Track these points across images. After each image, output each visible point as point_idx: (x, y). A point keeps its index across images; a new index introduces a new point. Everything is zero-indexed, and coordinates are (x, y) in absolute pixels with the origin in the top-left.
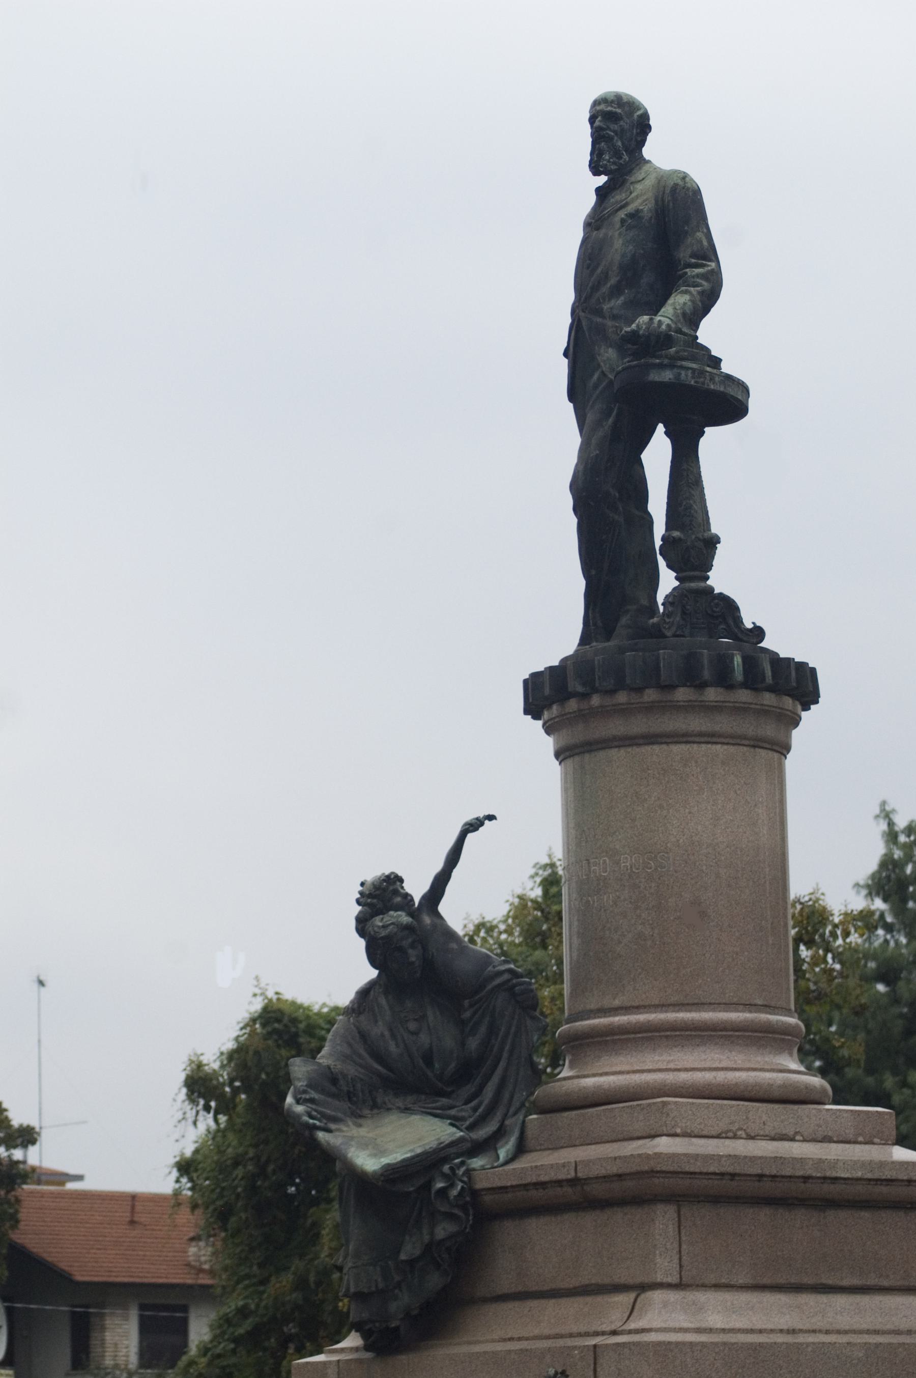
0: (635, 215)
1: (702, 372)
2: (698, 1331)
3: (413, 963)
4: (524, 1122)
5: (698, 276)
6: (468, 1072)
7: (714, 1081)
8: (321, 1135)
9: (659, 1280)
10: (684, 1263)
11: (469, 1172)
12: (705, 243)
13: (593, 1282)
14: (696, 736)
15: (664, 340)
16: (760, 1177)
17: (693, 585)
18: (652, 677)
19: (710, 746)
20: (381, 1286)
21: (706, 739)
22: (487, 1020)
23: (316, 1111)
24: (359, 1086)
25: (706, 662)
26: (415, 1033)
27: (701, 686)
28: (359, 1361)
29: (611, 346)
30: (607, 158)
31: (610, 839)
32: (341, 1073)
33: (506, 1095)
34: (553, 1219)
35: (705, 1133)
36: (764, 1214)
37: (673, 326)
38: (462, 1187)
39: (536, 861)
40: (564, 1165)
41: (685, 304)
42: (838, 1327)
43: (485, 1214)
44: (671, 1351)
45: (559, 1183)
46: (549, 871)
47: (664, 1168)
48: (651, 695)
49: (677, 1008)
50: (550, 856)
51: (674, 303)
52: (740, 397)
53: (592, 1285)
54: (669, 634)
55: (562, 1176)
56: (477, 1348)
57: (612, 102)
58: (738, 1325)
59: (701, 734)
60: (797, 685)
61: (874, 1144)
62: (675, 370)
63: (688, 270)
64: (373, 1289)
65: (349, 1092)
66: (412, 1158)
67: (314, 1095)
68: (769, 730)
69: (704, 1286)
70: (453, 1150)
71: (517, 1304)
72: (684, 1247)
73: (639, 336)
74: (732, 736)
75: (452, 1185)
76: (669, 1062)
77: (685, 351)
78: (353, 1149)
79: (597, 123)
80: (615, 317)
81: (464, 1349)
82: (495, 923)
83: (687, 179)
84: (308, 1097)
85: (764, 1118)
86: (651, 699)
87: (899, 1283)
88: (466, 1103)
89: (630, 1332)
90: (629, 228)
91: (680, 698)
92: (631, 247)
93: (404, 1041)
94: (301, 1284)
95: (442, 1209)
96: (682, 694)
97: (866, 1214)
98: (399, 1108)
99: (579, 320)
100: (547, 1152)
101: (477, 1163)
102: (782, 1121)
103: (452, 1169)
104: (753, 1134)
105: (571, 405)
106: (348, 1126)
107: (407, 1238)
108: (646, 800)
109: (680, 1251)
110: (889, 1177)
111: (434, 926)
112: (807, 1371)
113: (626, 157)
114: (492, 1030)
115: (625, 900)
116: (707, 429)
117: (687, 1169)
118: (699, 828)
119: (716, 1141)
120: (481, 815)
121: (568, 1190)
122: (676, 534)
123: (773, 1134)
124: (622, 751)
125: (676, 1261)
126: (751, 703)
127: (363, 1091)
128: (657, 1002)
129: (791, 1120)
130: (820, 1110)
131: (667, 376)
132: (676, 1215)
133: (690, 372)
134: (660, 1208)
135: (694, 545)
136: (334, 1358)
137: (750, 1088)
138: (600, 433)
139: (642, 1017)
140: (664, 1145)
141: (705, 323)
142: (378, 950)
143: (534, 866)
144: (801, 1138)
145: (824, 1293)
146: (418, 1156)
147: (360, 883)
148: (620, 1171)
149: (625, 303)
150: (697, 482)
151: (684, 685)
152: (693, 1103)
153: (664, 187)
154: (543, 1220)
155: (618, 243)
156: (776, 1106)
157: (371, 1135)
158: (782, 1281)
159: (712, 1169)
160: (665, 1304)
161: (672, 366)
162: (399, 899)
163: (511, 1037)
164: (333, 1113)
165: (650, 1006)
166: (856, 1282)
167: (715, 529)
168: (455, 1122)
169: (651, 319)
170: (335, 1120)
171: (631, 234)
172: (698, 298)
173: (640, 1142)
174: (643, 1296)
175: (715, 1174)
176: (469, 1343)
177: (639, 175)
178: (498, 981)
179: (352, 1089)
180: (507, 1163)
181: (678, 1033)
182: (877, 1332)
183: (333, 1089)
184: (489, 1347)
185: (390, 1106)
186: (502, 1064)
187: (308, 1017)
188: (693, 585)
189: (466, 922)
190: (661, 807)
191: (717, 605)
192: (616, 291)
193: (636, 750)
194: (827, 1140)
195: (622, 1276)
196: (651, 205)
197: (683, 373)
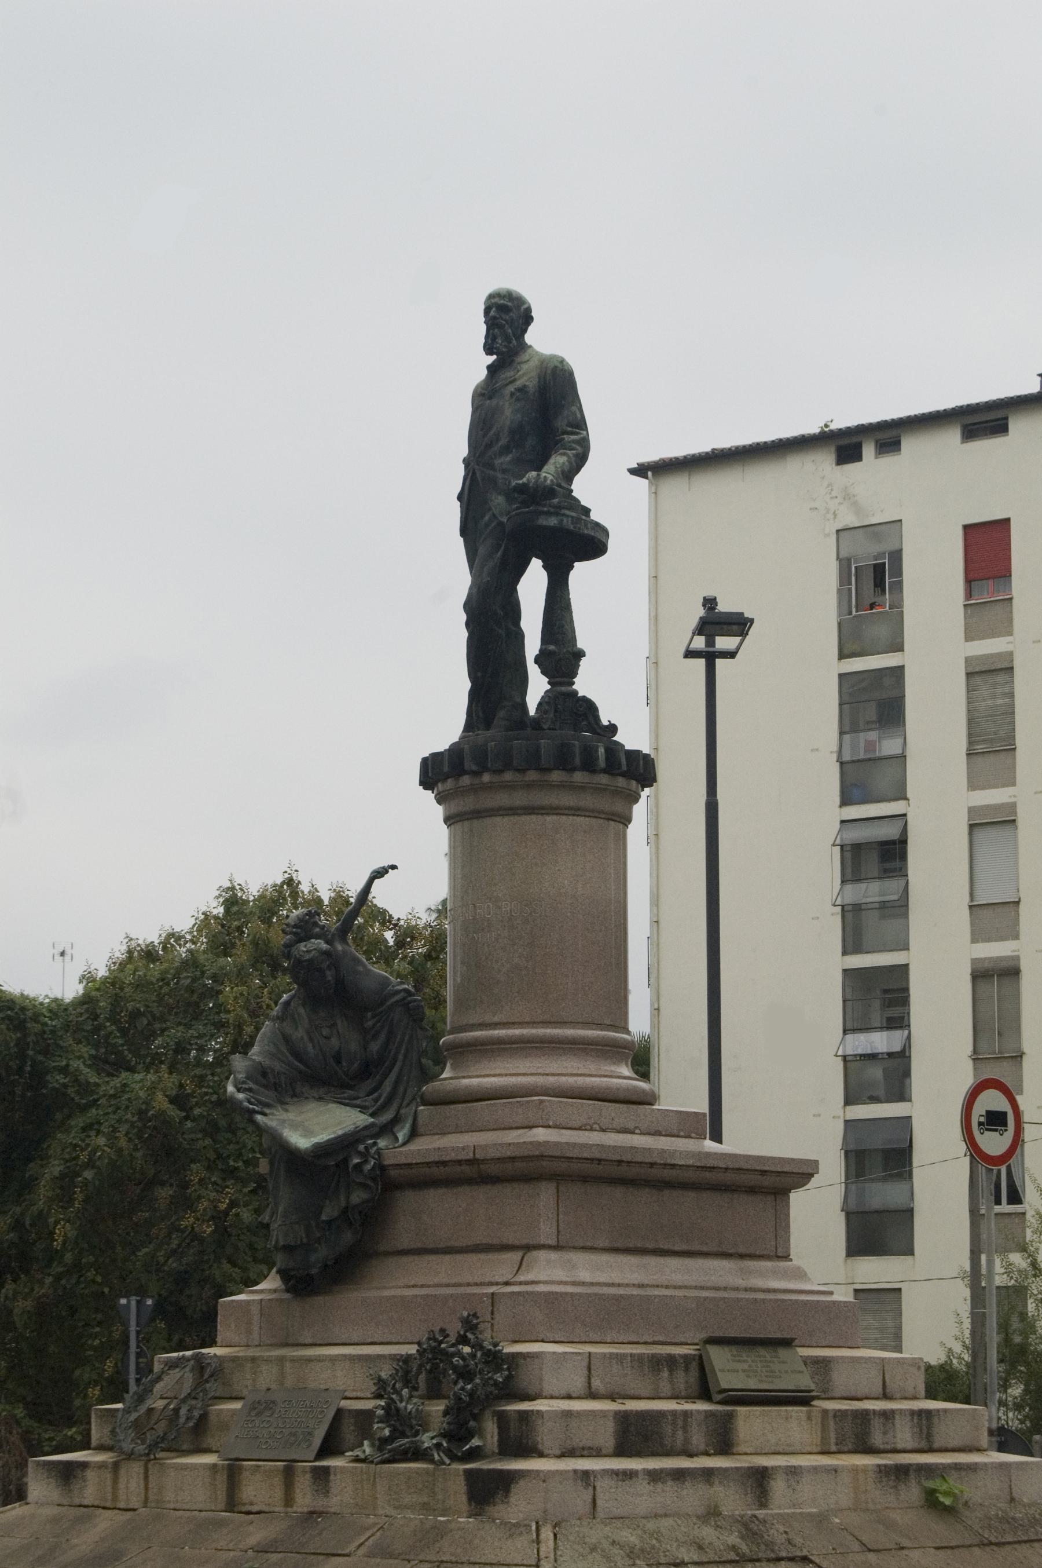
0: (522, 390)
1: (579, 519)
2: (574, 1284)
4: (416, 1111)
5: (574, 441)
11: (379, 1152)
12: (579, 415)
15: (549, 492)
17: (563, 689)
18: (533, 761)
24: (283, 1078)
25: (577, 751)
27: (573, 770)
28: (281, 1301)
29: (500, 494)
33: (401, 1089)
36: (619, 1192)
40: (463, 1148)
43: (390, 1183)
45: (459, 1162)
48: (532, 776)
54: (545, 727)
55: (462, 1156)
56: (386, 1293)
58: (602, 1280)
59: (570, 808)
62: (560, 518)
65: (275, 1083)
66: (335, 1138)
67: (251, 1085)
68: (618, 807)
70: (365, 1133)
72: (561, 1216)
74: (592, 811)
75: (366, 1161)
79: (492, 313)
80: (504, 471)
89: (521, 1283)
90: (518, 400)
94: (18, 1225)
96: (556, 776)
98: (314, 1097)
99: (474, 473)
100: (437, 1137)
101: (382, 1143)
108: (524, 859)
113: (514, 342)
116: (576, 564)
121: (466, 1168)
122: (552, 647)
124: (506, 818)
125: (555, 1227)
131: (553, 521)
134: (543, 1185)
135: (562, 656)
136: (257, 1297)
138: (491, 564)
139: (517, 1032)
140: (540, 1134)
141: (577, 479)
146: (339, 1137)
148: (513, 1155)
150: (567, 607)
151: (558, 769)
154: (441, 1191)
155: (508, 412)
156: (621, 1106)
157: (299, 1119)
159: (585, 1155)
161: (557, 514)
162: (318, 930)
166: (684, 1247)
167: (580, 644)
168: (363, 1109)
169: (539, 475)
170: (268, 1105)
172: (573, 459)
173: (520, 1131)
174: (529, 1254)
177: (525, 357)
178: (396, 998)
180: (404, 1144)
182: (702, 1288)
183: (264, 1082)
184: (399, 1292)
185: (306, 1095)
186: (399, 1064)
187: (34, 1006)
188: (563, 689)
190: (536, 864)
192: (506, 450)
194: (657, 1133)
195: (510, 1238)
196: (535, 382)
197: (565, 521)
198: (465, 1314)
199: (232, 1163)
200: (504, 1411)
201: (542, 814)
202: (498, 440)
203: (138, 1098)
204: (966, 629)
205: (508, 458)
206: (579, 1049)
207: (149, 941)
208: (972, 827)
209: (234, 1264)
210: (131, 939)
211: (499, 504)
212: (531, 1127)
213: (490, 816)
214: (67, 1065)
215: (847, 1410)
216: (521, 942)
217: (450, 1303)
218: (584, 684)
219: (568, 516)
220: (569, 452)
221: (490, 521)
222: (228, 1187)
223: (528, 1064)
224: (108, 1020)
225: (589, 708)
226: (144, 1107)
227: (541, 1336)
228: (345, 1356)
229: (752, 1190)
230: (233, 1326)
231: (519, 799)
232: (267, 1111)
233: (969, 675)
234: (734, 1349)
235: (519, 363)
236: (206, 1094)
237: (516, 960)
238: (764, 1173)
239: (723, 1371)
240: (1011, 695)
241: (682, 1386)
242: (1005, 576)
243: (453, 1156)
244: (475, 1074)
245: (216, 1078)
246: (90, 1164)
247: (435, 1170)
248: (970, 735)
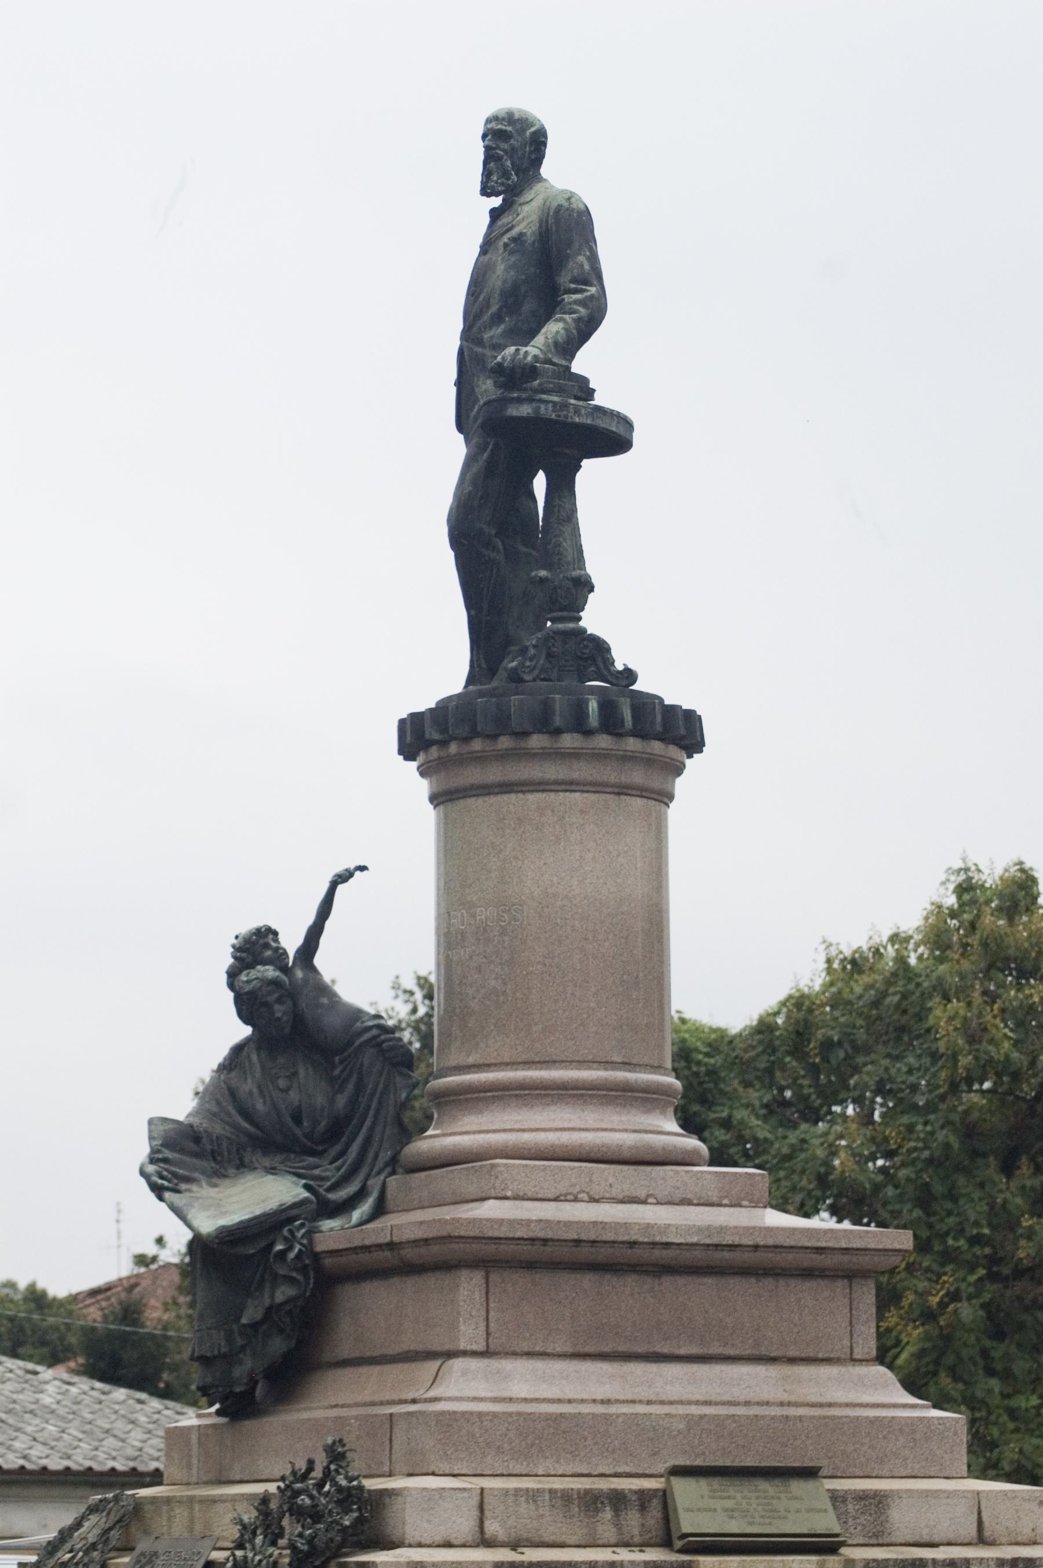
0: (518, 239)
1: (565, 406)
2: (495, 1400)
3: (279, 1019)
5: (576, 302)
6: (337, 1131)
7: (557, 1142)
9: (462, 1348)
10: (491, 1330)
13: (412, 1348)
15: (530, 371)
16: (578, 1242)
19: (568, 794)
20: (223, 1350)
23: (167, 1170)
24: (225, 1144)
26: (286, 1091)
27: (558, 732)
30: (495, 178)
31: (467, 891)
32: (206, 1131)
35: (540, 1196)
36: (587, 1280)
37: (541, 356)
38: (300, 1250)
39: (949, 866)
41: (557, 332)
42: (664, 1398)
43: (327, 1280)
44: (456, 1420)
45: (380, 1246)
46: (963, 877)
47: (462, 1233)
49: (514, 1067)
50: (964, 860)
51: (546, 333)
52: (614, 429)
54: (527, 678)
57: (503, 119)
59: (556, 782)
60: (683, 732)
61: (741, 1206)
62: (534, 405)
63: (565, 296)
64: (216, 1353)
65: (213, 1152)
67: (167, 1154)
69: (515, 1354)
72: (492, 1313)
74: (591, 784)
75: (290, 1248)
76: (516, 1122)
77: (550, 383)
78: (193, 1211)
81: (305, 1415)
82: (910, 933)
83: (573, 200)
84: (160, 1156)
85: (611, 1180)
86: (504, 746)
87: (747, 1352)
88: (332, 1163)
90: (511, 253)
91: (534, 746)
92: (512, 273)
93: (271, 1096)
95: (281, 1272)
96: (537, 741)
97: (709, 1281)
102: (632, 1184)
103: (291, 1231)
104: (597, 1197)
105: (462, 436)
106: (201, 1187)
107: (250, 1301)
108: (501, 851)
109: (487, 1319)
110: (730, 1242)
111: (306, 981)
112: (616, 1442)
113: (514, 177)
114: (359, 1088)
117: (490, 1234)
118: (555, 880)
119: (553, 1204)
120: (352, 866)
121: (387, 1254)
123: (621, 1196)
124: (480, 800)
126: (612, 750)
127: (229, 1153)
129: (642, 1183)
130: (677, 1172)
131: (525, 410)
132: (484, 1281)
133: (550, 405)
134: (464, 1274)
137: (595, 1149)
138: (475, 469)
140: (490, 1210)
141: (580, 355)
142: (247, 1005)
143: (947, 871)
144: (654, 1201)
145: (655, 1362)
148: (425, 1236)
151: (540, 732)
152: (527, 1165)
153: (549, 209)
155: (500, 268)
156: (625, 1168)
158: (606, 1349)
160: (465, 1373)
161: (530, 400)
163: (377, 1095)
164: (186, 1173)
165: (501, 1064)
169: (517, 350)
170: (188, 1180)
171: (513, 259)
172: (573, 325)
178: (367, 1036)
179: (216, 1148)
181: (527, 1092)
186: (368, 1123)
189: (871, 933)
190: (516, 858)
191: (586, 647)
196: (535, 227)
197: (543, 407)
198: (330, 1440)
199: (950, 1242)
200: (345, 1562)
201: (523, 792)
202: (488, 306)
203: (814, 1157)
206: (574, 1096)
207: (855, 947)
209: (956, 1378)
210: (831, 945)
213: (464, 797)
214: (730, 1117)
215: (887, 1560)
219: (547, 402)
220: (567, 317)
222: (945, 1274)
224: (788, 1053)
226: (822, 1170)
227: (432, 1468)
228: (243, 1495)
229: (809, 1273)
231: (494, 774)
234: (716, 1482)
235: (521, 204)
236: (915, 1149)
237: (493, 983)
238: (819, 1250)
239: (688, 1510)
241: (636, 1531)
245: (929, 1128)
247: (365, 1257)
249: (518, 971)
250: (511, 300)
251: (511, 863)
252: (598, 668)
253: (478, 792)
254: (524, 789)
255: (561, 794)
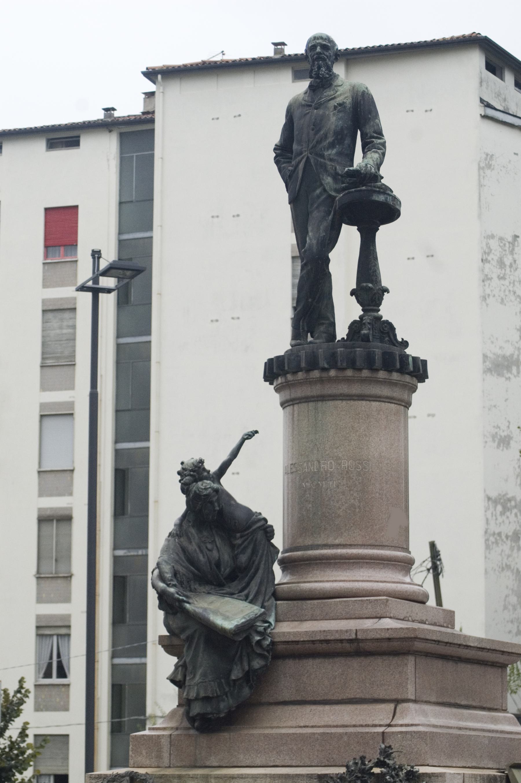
5: (380, 144)
8: (187, 606)
10: (417, 689)
14: (384, 398)
19: (389, 404)
21: (374, 399)
22: (251, 546)
29: (329, 175)
30: (324, 70)
31: (335, 450)
33: (263, 589)
34: (326, 661)
36: (439, 663)
40: (347, 631)
53: (356, 698)
57: (326, 39)
59: (387, 397)
62: (386, 196)
66: (246, 622)
71: (299, 707)
72: (417, 679)
73: (361, 173)
75: (264, 639)
80: (331, 160)
86: (366, 375)
90: (339, 111)
98: (204, 592)
108: (357, 431)
114: (254, 552)
115: (344, 485)
124: (344, 402)
125: (414, 687)
128: (361, 543)
147: (180, 462)
148: (391, 637)
149: (336, 153)
155: (333, 119)
167: (384, 283)
171: (341, 115)
175: (434, 641)
176: (262, 728)
181: (373, 561)
190: (366, 435)
192: (332, 145)
193: (352, 403)
204: (44, 279)
205: (334, 151)
206: (392, 565)
208: (42, 416)
211: (329, 183)
212: (380, 618)
213: (333, 400)
216: (355, 489)
217: (345, 738)
218: (387, 311)
220: (379, 151)
221: (321, 194)
223: (362, 574)
225: (388, 329)
230: (144, 752)
232: (190, 601)
233: (44, 311)
240: (74, 327)
242: (72, 245)
243: (337, 636)
244: (326, 579)
246: (263, 634)
248: (43, 353)
249: (367, 496)
250: (339, 137)
251: (363, 437)
252: (390, 339)
253: (344, 398)
254: (370, 399)
255: (387, 403)
